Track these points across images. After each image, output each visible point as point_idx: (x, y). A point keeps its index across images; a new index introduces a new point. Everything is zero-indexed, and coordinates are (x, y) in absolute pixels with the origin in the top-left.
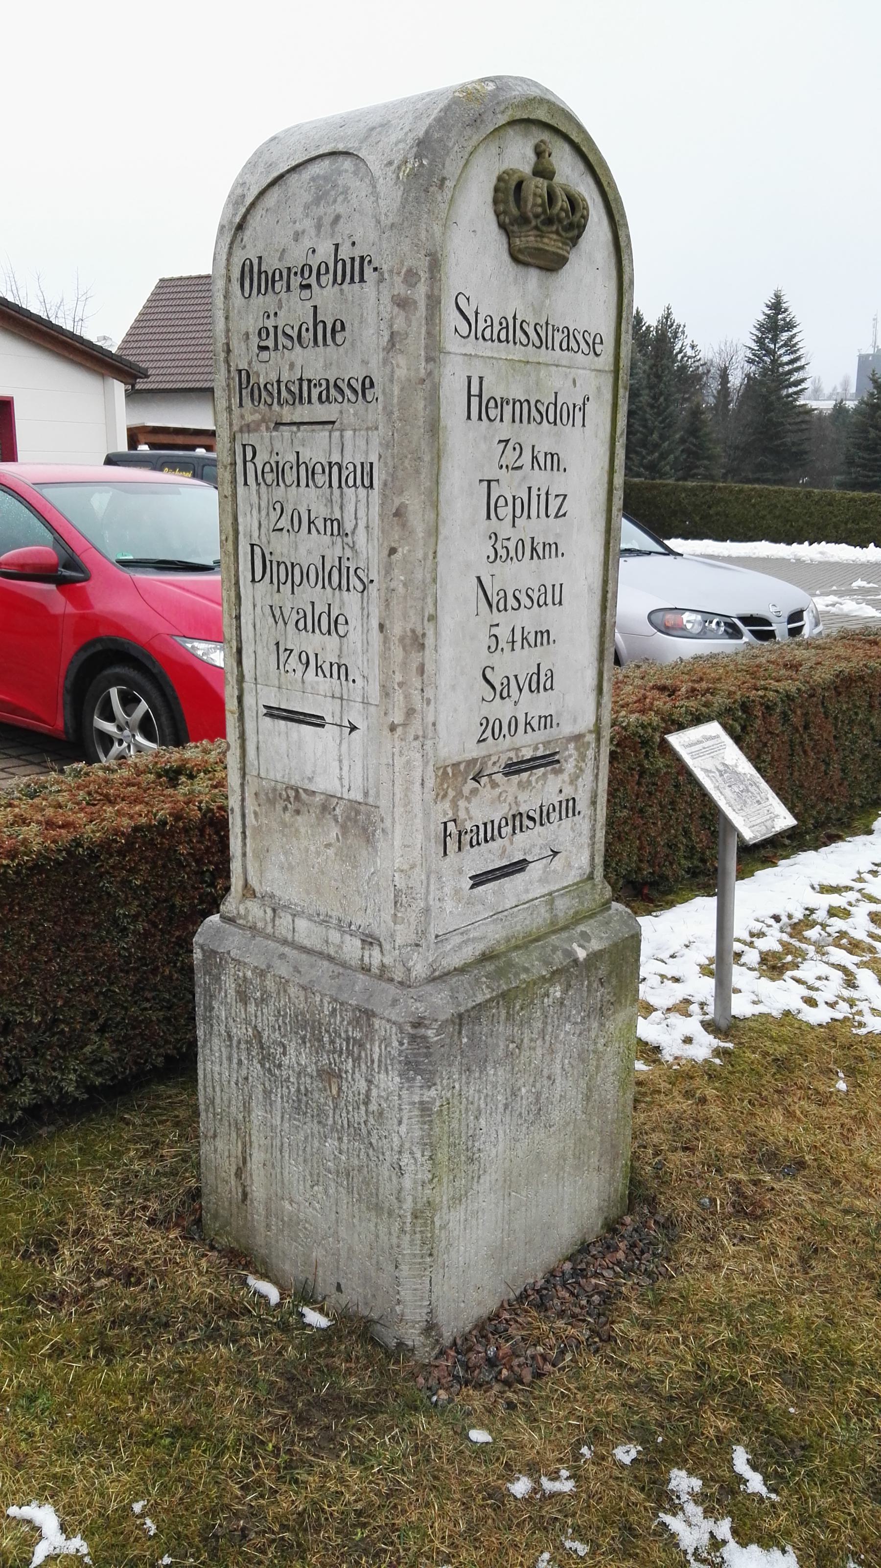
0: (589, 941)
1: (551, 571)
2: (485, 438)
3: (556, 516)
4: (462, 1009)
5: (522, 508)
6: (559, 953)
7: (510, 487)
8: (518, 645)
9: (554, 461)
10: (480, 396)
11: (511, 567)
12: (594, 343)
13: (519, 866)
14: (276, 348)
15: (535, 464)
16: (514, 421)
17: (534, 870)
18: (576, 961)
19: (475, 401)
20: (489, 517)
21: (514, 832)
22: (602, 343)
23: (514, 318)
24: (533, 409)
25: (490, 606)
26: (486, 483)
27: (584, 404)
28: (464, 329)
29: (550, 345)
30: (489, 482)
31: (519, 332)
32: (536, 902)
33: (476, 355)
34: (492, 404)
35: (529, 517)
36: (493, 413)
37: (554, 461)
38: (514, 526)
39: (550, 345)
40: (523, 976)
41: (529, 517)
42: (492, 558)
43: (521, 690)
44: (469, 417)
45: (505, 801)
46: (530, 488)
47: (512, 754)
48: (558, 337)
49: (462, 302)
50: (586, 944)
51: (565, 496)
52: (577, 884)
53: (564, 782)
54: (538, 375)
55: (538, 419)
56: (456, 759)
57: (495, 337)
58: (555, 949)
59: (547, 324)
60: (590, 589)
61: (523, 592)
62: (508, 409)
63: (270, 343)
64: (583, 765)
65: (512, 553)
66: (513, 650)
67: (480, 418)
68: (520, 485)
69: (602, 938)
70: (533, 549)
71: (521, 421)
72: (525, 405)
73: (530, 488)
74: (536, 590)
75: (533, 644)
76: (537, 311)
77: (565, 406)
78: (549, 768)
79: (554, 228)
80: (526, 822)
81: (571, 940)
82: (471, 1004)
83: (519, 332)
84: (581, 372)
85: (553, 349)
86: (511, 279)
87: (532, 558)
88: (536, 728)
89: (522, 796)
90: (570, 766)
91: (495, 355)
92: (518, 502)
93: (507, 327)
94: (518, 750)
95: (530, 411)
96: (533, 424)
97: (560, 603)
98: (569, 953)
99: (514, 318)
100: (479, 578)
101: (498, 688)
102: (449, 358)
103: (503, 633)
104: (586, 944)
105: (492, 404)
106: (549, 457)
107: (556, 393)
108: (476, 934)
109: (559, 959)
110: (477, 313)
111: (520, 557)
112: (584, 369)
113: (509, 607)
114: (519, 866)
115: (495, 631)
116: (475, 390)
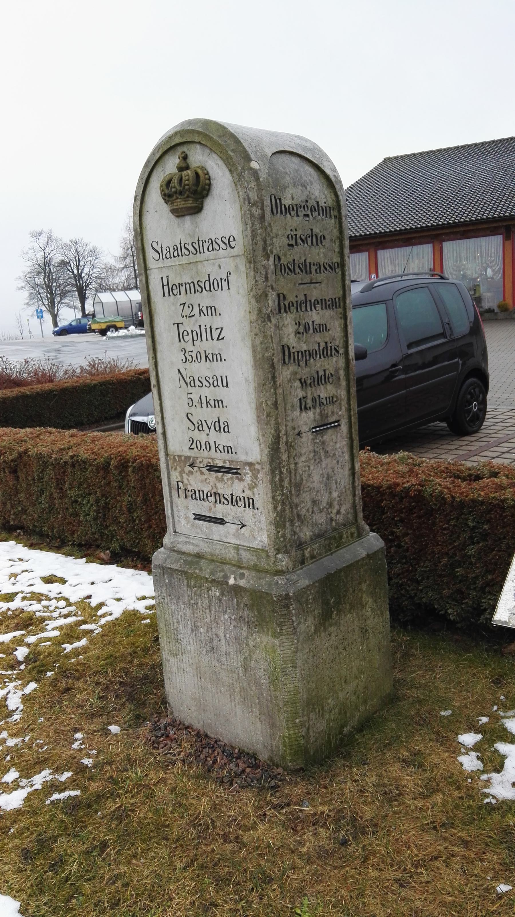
0: (241, 579)
1: (219, 369)
2: (173, 304)
3: (218, 339)
4: (164, 565)
5: (197, 336)
6: (222, 574)
7: (188, 326)
8: (204, 405)
9: (213, 311)
10: (168, 285)
11: (195, 366)
12: (229, 242)
13: (221, 521)
14: (296, 244)
15: (202, 314)
16: (186, 293)
17: (231, 528)
18: (227, 583)
19: (166, 288)
20: (180, 341)
21: (216, 502)
22: (234, 240)
23: (180, 244)
24: (196, 286)
25: (186, 384)
26: (176, 325)
27: (227, 277)
28: (157, 256)
29: (202, 251)
30: (178, 324)
31: (184, 250)
32: (228, 545)
33: (164, 267)
34: (174, 287)
35: (202, 340)
36: (175, 292)
37: (213, 311)
38: (194, 345)
39: (202, 251)
40: (197, 571)
41: (202, 340)
42: (184, 361)
43: (209, 429)
44: (164, 295)
45: (209, 483)
46: (200, 326)
47: (210, 461)
48: (206, 246)
49: (155, 245)
50: (238, 579)
51: (222, 328)
52: (257, 549)
53: (245, 487)
54: (197, 268)
55: (200, 290)
56: (179, 453)
57: (172, 255)
58: (223, 571)
59: (198, 241)
60: (246, 380)
61: (204, 378)
62: (183, 289)
63: (293, 242)
64: (257, 481)
65: (195, 358)
66: (202, 407)
67: (169, 295)
68: (194, 324)
69: (249, 582)
70: (206, 357)
71: (191, 293)
72: (192, 285)
73: (200, 326)
74: (211, 378)
75: (213, 406)
76: (191, 236)
77: (215, 281)
78: (235, 476)
79: (175, 197)
80: (223, 500)
81: (233, 572)
82: (168, 566)
83: (184, 250)
84: (223, 260)
85: (204, 252)
86: (176, 225)
87: (206, 361)
88: (222, 451)
89: (219, 485)
90: (248, 478)
91: (173, 264)
92: (194, 333)
93: (177, 250)
94: (213, 459)
95: (196, 287)
96: (197, 293)
97: (227, 386)
98: (226, 577)
99: (180, 244)
100: (179, 370)
101: (197, 425)
102: (152, 271)
103: (195, 397)
104: (238, 579)
105: (174, 287)
106: (209, 309)
107: (209, 275)
108: (194, 542)
109: (219, 576)
110: (162, 247)
111: (199, 360)
112: (225, 257)
113: (196, 385)
114: (221, 521)
115: (190, 396)
116: (165, 283)
